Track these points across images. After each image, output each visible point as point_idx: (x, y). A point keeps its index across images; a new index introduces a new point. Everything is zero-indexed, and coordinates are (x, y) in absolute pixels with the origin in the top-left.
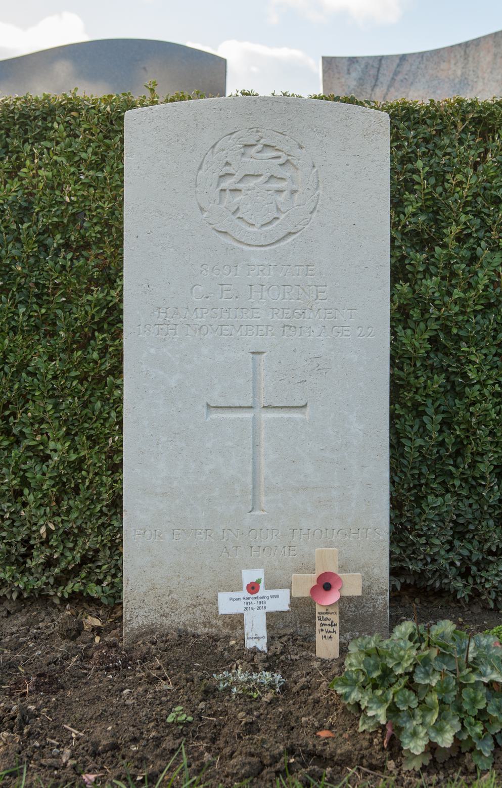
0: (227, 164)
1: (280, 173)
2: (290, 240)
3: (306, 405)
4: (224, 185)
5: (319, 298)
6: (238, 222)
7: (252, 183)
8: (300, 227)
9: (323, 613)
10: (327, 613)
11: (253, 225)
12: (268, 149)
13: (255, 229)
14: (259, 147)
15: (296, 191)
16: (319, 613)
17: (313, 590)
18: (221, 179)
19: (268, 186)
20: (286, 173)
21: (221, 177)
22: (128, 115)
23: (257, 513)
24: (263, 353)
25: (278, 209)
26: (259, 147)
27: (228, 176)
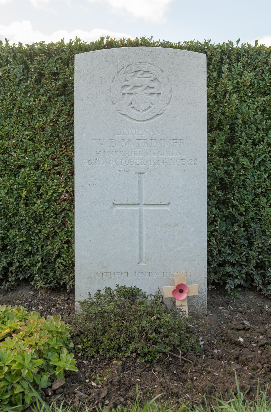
0: (126, 80)
1: (152, 84)
3: (169, 204)
4: (124, 91)
6: (132, 110)
8: (161, 111)
9: (179, 306)
10: (181, 306)
12: (147, 73)
13: (140, 113)
14: (141, 72)
16: (178, 306)
17: (174, 292)
18: (145, 73)
19: (146, 91)
20: (155, 84)
21: (122, 87)
22: (78, 57)
23: (142, 264)
25: (151, 103)
26: (141, 72)
27: (126, 87)
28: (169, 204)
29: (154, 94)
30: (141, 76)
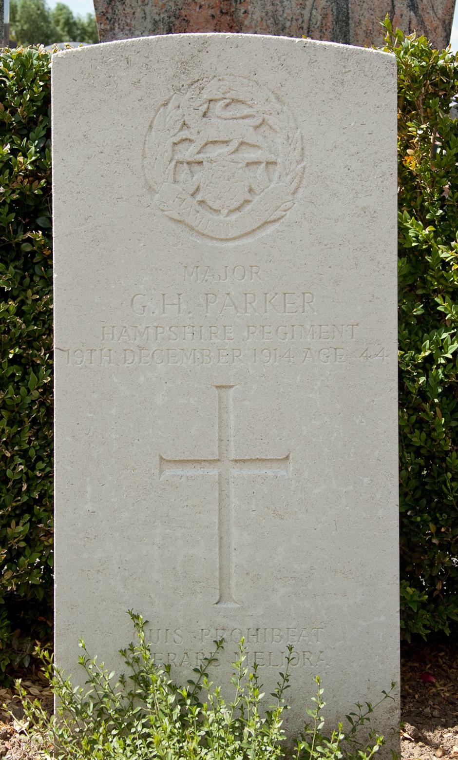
3: (287, 458)
11: (217, 211)
24: (231, 387)
28: (287, 458)
29: (258, 163)
30: (228, 114)
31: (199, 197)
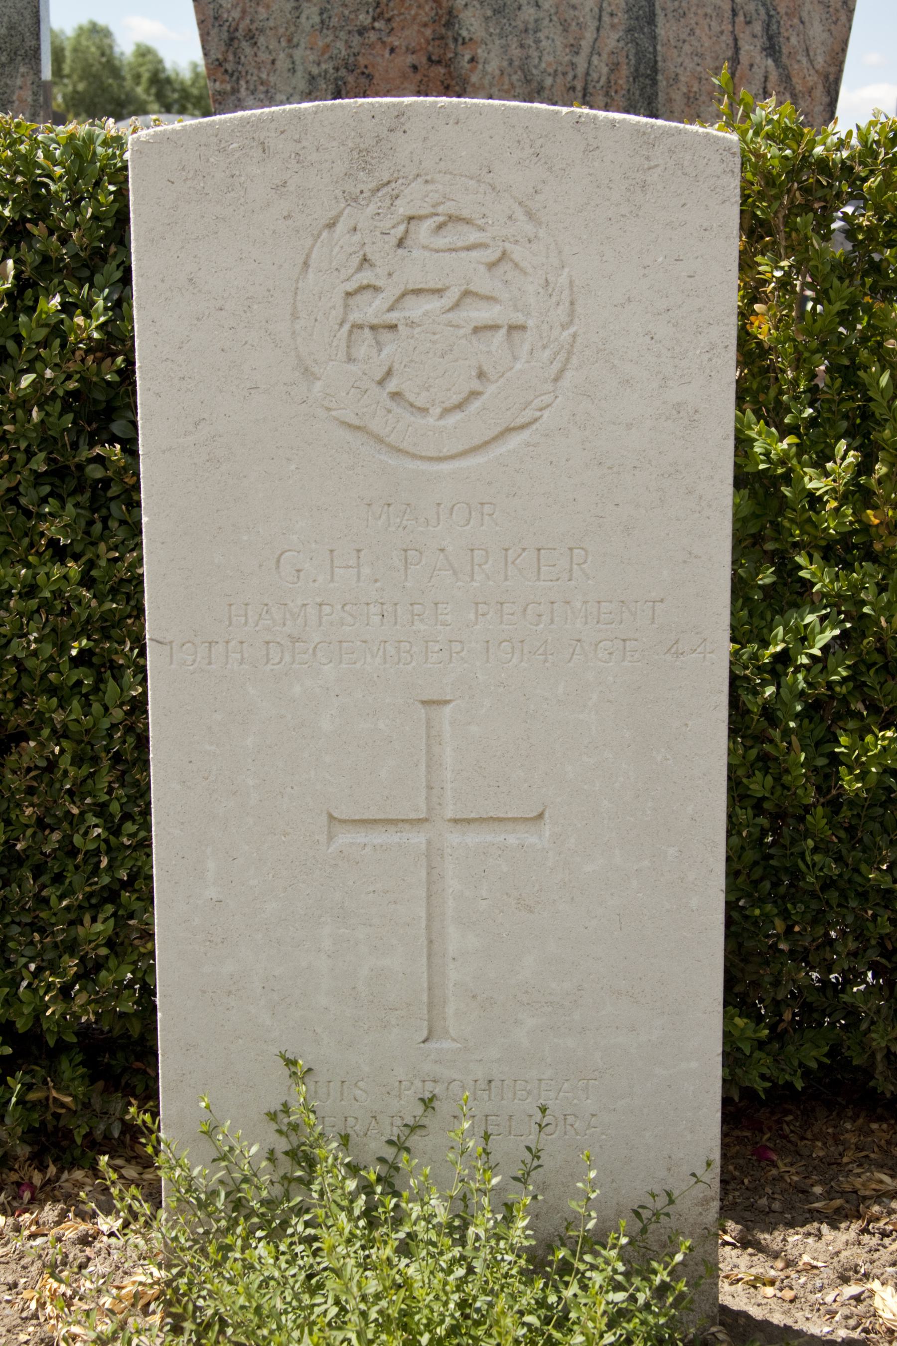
1: (483, 283)
2: (515, 441)
3: (541, 816)
5: (403, 661)
7: (417, 308)
15: (523, 328)
24: (447, 702)
28: (541, 816)
31: (392, 385)
